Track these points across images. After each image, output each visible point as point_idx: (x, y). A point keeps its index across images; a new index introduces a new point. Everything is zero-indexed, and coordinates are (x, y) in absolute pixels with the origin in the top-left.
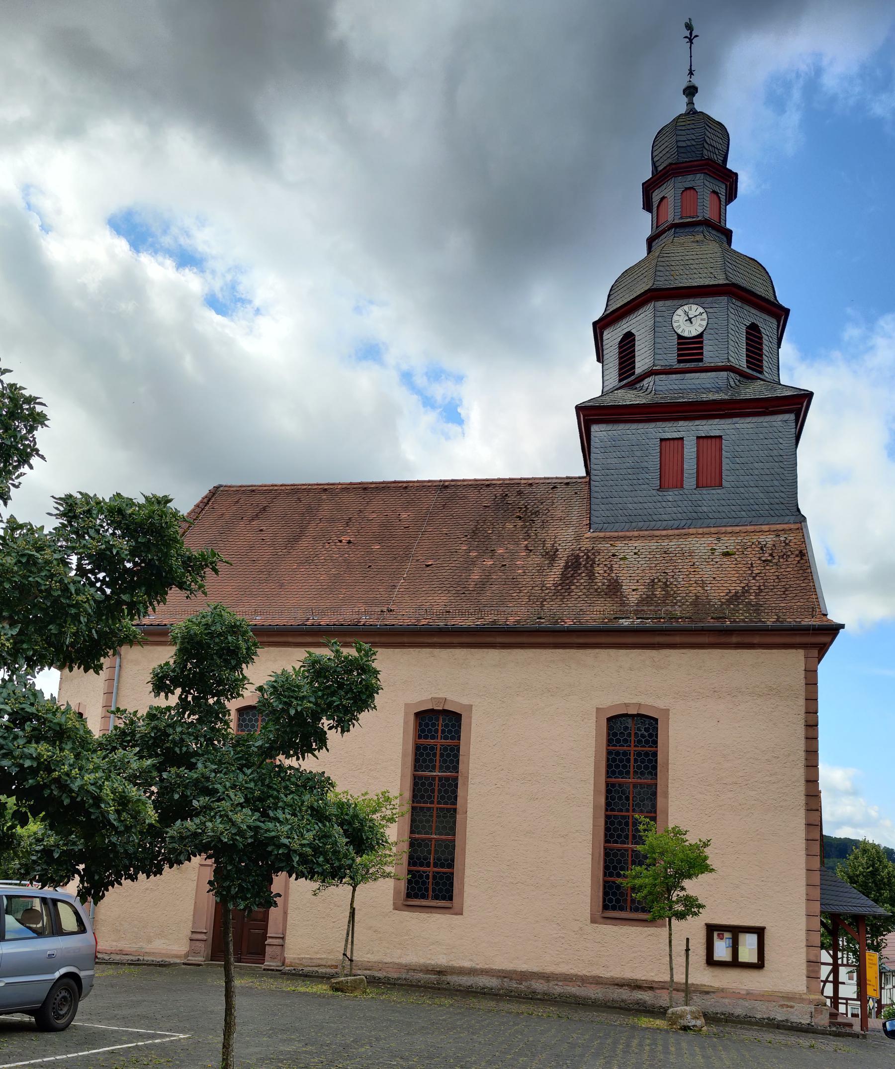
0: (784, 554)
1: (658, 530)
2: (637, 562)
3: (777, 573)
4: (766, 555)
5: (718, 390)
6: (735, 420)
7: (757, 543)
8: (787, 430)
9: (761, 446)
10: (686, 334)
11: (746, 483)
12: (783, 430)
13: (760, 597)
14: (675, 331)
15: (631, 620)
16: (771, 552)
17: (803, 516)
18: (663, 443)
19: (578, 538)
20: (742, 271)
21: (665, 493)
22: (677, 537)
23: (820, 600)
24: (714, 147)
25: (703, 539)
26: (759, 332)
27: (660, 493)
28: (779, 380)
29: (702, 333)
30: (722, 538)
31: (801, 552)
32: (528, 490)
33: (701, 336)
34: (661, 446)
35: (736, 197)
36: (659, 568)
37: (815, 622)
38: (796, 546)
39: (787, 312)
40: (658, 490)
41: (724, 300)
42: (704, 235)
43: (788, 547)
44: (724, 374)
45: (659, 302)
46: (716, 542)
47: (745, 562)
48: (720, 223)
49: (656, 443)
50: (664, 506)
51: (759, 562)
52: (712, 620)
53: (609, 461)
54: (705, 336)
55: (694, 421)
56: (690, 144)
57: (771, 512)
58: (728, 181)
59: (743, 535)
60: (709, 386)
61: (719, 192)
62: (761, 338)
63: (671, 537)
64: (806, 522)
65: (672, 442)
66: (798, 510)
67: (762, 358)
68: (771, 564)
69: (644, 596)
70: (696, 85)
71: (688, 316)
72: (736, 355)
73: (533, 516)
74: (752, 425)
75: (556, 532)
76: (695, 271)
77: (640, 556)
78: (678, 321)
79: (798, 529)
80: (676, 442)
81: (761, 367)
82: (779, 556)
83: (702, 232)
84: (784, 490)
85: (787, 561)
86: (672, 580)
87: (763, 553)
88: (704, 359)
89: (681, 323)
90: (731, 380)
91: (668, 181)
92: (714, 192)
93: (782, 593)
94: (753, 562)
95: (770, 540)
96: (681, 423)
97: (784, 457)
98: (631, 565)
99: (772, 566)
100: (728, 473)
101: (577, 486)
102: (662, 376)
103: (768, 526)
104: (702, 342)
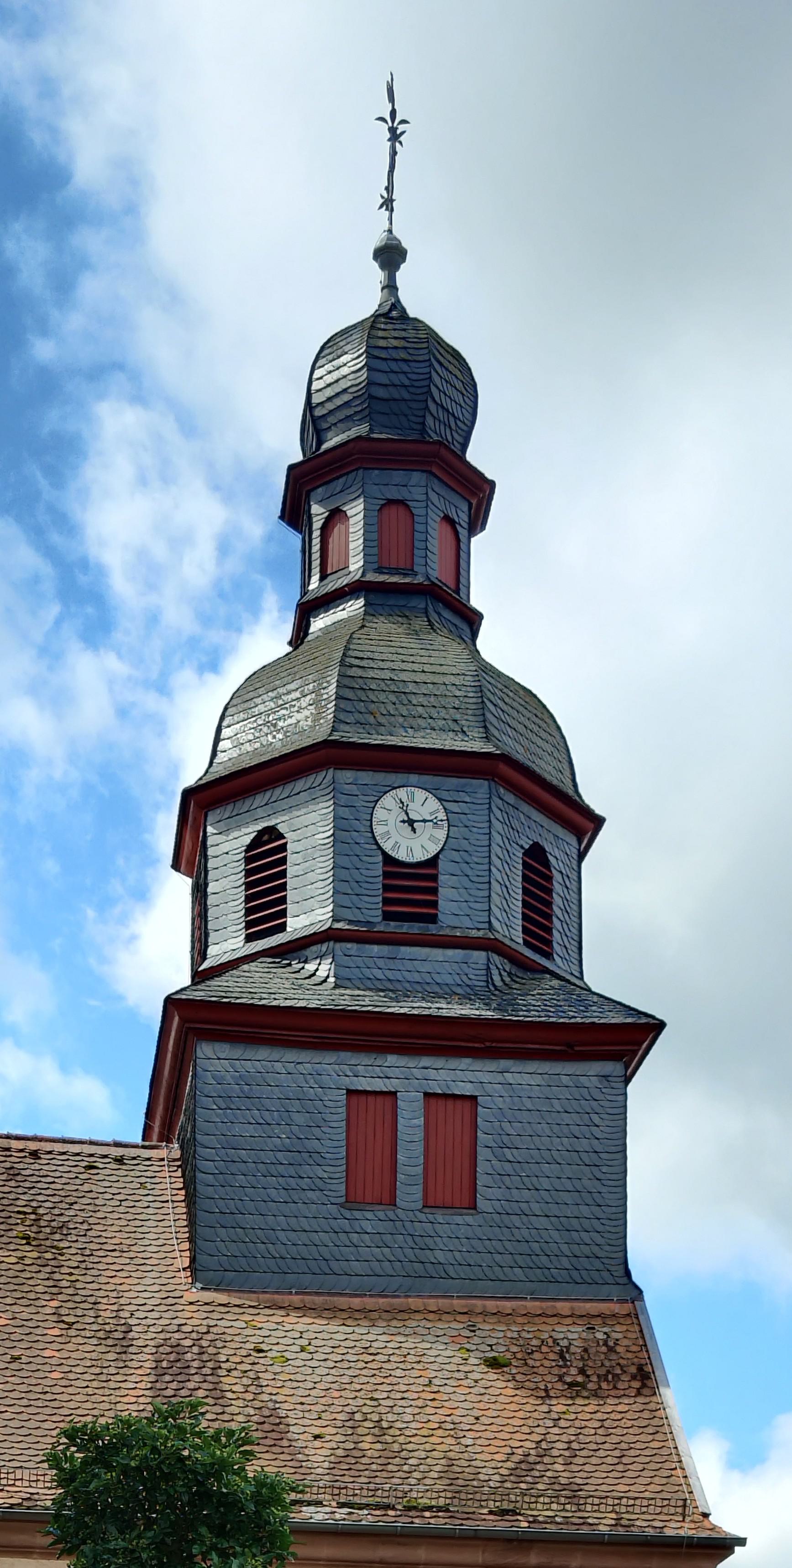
0: (608, 1372)
1: (341, 1295)
2: (310, 1371)
3: (599, 1416)
4: (573, 1371)
5: (469, 990)
6: (504, 1063)
7: (551, 1343)
8: (609, 1098)
9: (556, 1128)
10: (402, 855)
11: (524, 1206)
12: (601, 1097)
13: (575, 1468)
14: (377, 843)
15: (328, 1509)
16: (581, 1365)
17: (637, 1287)
18: (354, 1099)
19: (171, 1301)
20: (514, 723)
21: (357, 1214)
22: (385, 1316)
23: (691, 1481)
24: (448, 411)
25: (440, 1325)
26: (547, 864)
27: (347, 1214)
28: (581, 973)
29: (436, 857)
30: (479, 1326)
31: (640, 1368)
32: (29, 1167)
33: (433, 862)
34: (348, 1106)
35: (483, 528)
36: (358, 1387)
37: (686, 1530)
38: (629, 1355)
39: (598, 822)
40: (342, 1205)
41: (481, 787)
42: (429, 621)
43: (614, 1356)
44: (480, 956)
45: (344, 772)
46: (467, 1333)
47: (532, 1386)
48: (458, 594)
49: (339, 1098)
50: (355, 1241)
51: (559, 1386)
52: (492, 1517)
53: (237, 1129)
54: (441, 864)
55: (417, 1058)
56: (397, 396)
57: (575, 1274)
58: (474, 494)
59: (520, 1320)
60: (449, 980)
61: (457, 520)
62: (549, 879)
63: (375, 1315)
64: (642, 1300)
65: (371, 1099)
66: (628, 1273)
67: (551, 922)
68: (585, 1394)
69: (340, 1452)
70: (404, 244)
71: (407, 814)
72: (504, 914)
73: (57, 1237)
74: (538, 1080)
75: (116, 1281)
76: (420, 709)
77: (315, 1356)
78: (385, 823)
79: (629, 1315)
80: (380, 1099)
81: (549, 943)
82: (599, 1376)
83: (426, 612)
84: (600, 1228)
85: (615, 1388)
86: (391, 1417)
87: (566, 1366)
88: (440, 916)
89: (391, 827)
90: (495, 972)
91: (347, 474)
92: (447, 519)
93: (616, 1461)
94: (550, 1386)
95: (576, 1336)
96: (392, 1059)
97: (603, 1156)
98: (299, 1377)
99: (588, 1398)
100: (488, 1180)
101: (141, 1168)
102: (349, 945)
103: (567, 1305)
104: (434, 878)
